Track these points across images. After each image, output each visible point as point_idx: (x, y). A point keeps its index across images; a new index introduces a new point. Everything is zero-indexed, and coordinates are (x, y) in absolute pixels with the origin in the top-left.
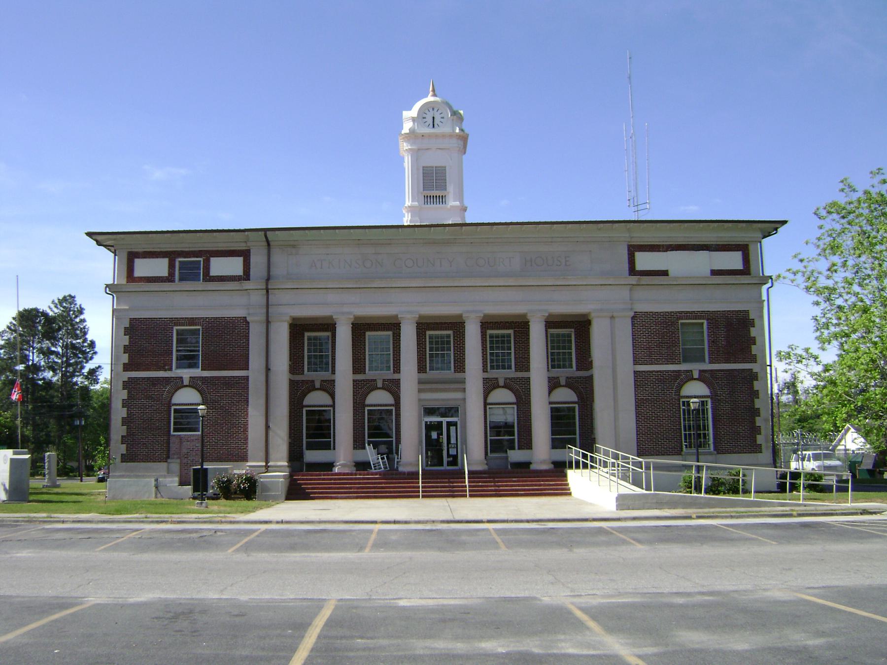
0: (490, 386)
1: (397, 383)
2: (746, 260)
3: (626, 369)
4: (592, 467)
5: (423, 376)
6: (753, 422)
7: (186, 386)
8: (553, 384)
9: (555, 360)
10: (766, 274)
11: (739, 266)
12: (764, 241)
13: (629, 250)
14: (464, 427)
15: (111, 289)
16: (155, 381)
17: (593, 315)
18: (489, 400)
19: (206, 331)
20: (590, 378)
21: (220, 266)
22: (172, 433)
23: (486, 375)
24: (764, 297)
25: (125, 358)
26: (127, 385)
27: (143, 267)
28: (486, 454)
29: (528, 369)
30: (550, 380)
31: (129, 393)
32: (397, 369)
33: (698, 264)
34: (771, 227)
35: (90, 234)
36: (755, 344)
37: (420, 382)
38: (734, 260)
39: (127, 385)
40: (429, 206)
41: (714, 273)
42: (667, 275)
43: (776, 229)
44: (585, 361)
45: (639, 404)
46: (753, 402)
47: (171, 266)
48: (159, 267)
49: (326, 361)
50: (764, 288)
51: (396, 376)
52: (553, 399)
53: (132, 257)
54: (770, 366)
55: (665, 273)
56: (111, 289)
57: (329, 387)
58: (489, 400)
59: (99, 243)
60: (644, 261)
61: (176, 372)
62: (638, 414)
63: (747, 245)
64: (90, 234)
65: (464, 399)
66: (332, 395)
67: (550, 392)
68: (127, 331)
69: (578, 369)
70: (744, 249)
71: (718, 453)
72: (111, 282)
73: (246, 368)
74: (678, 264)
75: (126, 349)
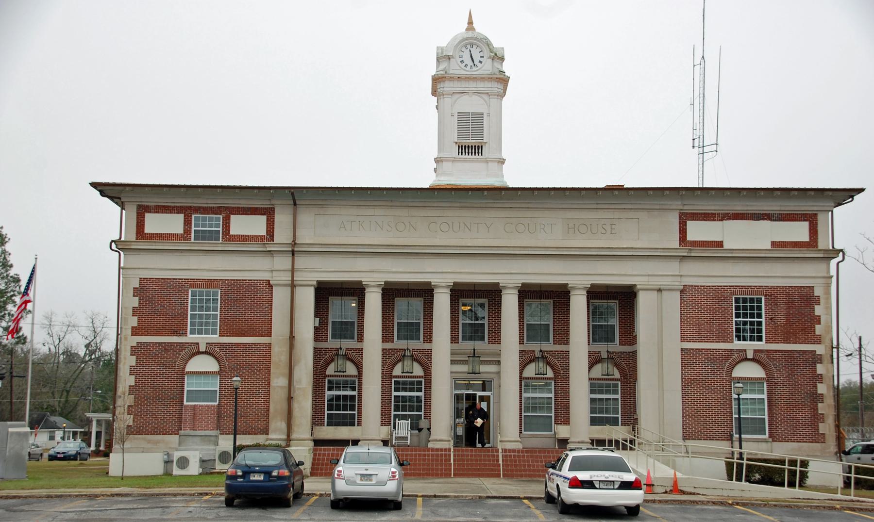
0: (526, 359)
1: (428, 353)
2: (813, 231)
3: (674, 346)
4: (631, 449)
5: (455, 346)
6: (816, 409)
7: (203, 353)
8: (594, 360)
9: (598, 333)
10: (837, 247)
11: (805, 237)
12: (836, 210)
13: (680, 217)
14: (498, 402)
15: (119, 245)
16: (167, 346)
17: (638, 287)
18: (525, 375)
19: (224, 294)
20: (634, 353)
21: (240, 225)
22: (185, 403)
23: (523, 348)
24: (833, 272)
25: (134, 321)
26: (134, 350)
27: (155, 223)
28: (521, 433)
29: (567, 342)
30: (591, 354)
31: (137, 358)
32: (429, 338)
33: (756, 235)
34: (847, 194)
35: (94, 185)
36: (819, 323)
37: (453, 354)
38: (799, 231)
39: (134, 350)
40: (463, 156)
41: (774, 244)
42: (722, 246)
43: (852, 197)
44: (629, 335)
45: (686, 384)
46: (816, 387)
47: (187, 223)
48: (173, 224)
49: (352, 329)
50: (833, 262)
51: (427, 346)
52: (592, 376)
53: (142, 211)
54: (838, 348)
55: (720, 244)
56: (119, 245)
57: (356, 358)
58: (525, 375)
59: (103, 194)
60: (697, 231)
61: (191, 338)
62: (684, 395)
63: (816, 215)
64: (94, 185)
65: (499, 373)
66: (359, 366)
67: (590, 368)
68: (137, 292)
69: (621, 344)
70: (812, 219)
71: (773, 441)
72: (117, 238)
73: (269, 335)
74: (739, 235)
75: (135, 312)
